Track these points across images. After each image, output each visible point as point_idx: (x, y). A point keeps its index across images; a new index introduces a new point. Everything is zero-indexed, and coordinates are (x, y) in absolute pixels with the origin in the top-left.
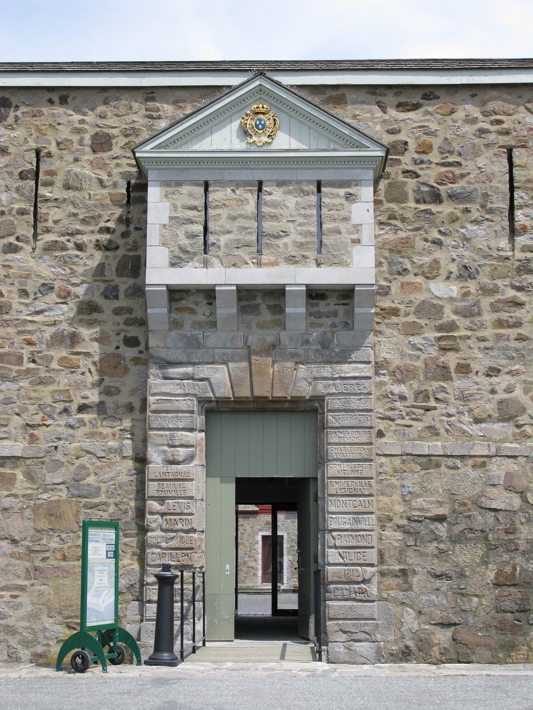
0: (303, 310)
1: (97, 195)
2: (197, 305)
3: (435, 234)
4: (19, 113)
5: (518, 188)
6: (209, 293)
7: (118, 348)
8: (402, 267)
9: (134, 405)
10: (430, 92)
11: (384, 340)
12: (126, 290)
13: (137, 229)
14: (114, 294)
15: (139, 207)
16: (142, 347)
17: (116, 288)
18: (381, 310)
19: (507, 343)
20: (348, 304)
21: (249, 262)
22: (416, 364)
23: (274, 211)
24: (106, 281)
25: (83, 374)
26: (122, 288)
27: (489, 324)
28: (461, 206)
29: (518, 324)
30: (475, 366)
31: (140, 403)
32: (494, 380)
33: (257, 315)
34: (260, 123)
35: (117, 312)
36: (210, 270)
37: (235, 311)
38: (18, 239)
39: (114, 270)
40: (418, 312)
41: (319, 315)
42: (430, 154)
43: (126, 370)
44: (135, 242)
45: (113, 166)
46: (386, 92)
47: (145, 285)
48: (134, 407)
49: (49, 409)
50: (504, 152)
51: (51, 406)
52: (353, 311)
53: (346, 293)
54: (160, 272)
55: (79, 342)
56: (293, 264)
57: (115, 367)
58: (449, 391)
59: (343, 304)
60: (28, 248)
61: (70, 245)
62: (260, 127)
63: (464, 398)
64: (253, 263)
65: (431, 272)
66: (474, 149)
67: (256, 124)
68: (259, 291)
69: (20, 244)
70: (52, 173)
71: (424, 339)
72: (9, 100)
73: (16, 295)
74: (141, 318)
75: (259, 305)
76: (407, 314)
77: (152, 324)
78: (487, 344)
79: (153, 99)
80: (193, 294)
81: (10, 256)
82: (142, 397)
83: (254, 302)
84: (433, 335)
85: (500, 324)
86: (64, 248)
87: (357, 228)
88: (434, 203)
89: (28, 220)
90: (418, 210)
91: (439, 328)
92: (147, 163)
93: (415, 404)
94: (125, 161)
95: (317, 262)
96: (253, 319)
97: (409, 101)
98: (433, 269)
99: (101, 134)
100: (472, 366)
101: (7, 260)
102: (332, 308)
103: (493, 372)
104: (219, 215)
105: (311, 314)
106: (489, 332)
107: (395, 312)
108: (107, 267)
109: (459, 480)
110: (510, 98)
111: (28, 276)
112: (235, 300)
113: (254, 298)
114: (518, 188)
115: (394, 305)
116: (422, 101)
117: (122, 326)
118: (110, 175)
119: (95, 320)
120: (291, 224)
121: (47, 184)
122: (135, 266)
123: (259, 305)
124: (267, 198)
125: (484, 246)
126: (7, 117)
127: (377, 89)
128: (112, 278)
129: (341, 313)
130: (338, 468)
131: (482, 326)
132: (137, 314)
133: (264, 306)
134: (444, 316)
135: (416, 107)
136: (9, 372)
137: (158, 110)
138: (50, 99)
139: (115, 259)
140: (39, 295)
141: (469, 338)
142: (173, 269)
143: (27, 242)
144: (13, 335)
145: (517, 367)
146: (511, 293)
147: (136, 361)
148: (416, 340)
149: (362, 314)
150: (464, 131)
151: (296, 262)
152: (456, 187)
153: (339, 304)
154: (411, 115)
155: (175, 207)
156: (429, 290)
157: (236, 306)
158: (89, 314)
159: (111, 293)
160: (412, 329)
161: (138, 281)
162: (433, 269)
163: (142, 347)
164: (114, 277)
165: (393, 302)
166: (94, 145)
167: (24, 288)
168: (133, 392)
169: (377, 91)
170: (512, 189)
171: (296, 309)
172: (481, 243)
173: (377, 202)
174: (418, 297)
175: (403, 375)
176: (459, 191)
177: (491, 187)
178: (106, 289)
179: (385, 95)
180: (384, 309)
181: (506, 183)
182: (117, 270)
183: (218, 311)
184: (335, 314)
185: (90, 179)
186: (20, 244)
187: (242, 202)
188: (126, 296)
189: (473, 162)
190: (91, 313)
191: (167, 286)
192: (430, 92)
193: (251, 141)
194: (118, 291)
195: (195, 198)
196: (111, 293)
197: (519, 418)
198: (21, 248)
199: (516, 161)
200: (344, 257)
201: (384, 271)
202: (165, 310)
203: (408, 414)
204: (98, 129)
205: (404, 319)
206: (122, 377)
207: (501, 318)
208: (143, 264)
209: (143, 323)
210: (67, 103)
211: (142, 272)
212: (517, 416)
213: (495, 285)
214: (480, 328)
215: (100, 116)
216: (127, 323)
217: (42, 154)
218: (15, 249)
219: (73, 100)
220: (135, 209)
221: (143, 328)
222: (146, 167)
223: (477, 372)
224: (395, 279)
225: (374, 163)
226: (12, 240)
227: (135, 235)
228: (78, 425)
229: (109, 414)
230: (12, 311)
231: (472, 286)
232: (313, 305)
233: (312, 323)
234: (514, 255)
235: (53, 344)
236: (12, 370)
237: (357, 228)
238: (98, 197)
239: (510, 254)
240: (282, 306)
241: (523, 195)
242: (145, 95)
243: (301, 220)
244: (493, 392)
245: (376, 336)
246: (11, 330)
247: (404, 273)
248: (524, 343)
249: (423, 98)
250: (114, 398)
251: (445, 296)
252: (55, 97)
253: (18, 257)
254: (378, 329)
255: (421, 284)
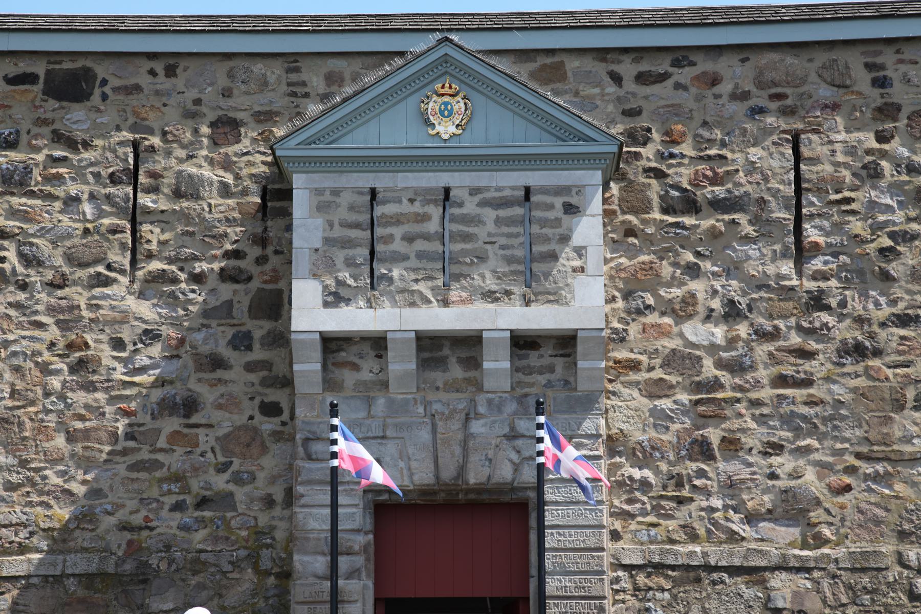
0: (507, 365)
1: (220, 205)
2: (361, 358)
3: (690, 257)
4: (107, 89)
5: (808, 190)
6: (378, 343)
7: (251, 418)
8: (643, 302)
9: (274, 497)
10: (683, 57)
11: (620, 404)
12: (263, 337)
13: (277, 252)
14: (246, 343)
15: (281, 222)
16: (285, 416)
17: (248, 336)
18: (615, 362)
19: (792, 407)
20: (569, 356)
21: (433, 299)
22: (664, 437)
23: (466, 229)
24: (234, 325)
25: (202, 455)
26: (257, 334)
27: (765, 381)
28: (726, 217)
29: (807, 383)
30: (747, 441)
31: (283, 495)
32: (776, 460)
33: (444, 372)
34: (446, 109)
35: (250, 367)
36: (379, 311)
37: (414, 367)
38: (109, 267)
39: (246, 309)
40: (665, 365)
41: (529, 371)
42: (684, 145)
43: (264, 450)
44: (274, 270)
45: (242, 165)
46: (622, 57)
47: (290, 332)
48: (274, 501)
49: (154, 505)
50: (787, 140)
51: (158, 501)
52: (575, 364)
53: (566, 342)
54: (311, 312)
55: (197, 411)
56: (492, 302)
57: (248, 445)
58: (711, 475)
59: (562, 355)
60: (124, 280)
61: (183, 276)
62: (446, 113)
63: (731, 486)
64: (438, 301)
65: (684, 310)
66: (745, 136)
67: (440, 109)
68: (445, 338)
69: (113, 275)
70: (154, 175)
71: (675, 402)
72: (93, 71)
73: (106, 347)
74: (284, 376)
75: (447, 357)
76: (651, 369)
77: (300, 386)
78: (766, 411)
79: (297, 70)
80: (356, 343)
81: (97, 291)
82: (285, 486)
83: (440, 353)
84: (684, 397)
85: (781, 381)
86: (175, 281)
87: (580, 251)
88: (688, 212)
89: (124, 241)
90: (665, 223)
91: (698, 387)
92: (291, 165)
93: (663, 493)
94: (259, 158)
95: (525, 299)
96: (438, 377)
97: (653, 69)
98: (688, 304)
99: (224, 119)
100: (743, 440)
101: (94, 297)
102: (546, 361)
103: (775, 448)
104: (392, 235)
105: (518, 370)
106: (766, 393)
107: (634, 366)
108: (236, 306)
109: (727, 602)
110: (796, 62)
111: (124, 322)
112: (414, 352)
113: (440, 348)
114: (808, 190)
115: (633, 356)
116: (671, 70)
117: (259, 388)
118: (237, 177)
119: (219, 380)
120: (488, 247)
121: (148, 191)
122: (275, 305)
123: (447, 357)
124: (456, 211)
125: (758, 272)
126: (91, 94)
127: (608, 53)
128: (243, 321)
129: (559, 369)
130: (557, 584)
131: (757, 384)
132: (280, 369)
133: (453, 360)
134: (704, 370)
135: (663, 78)
136: (97, 455)
137: (304, 84)
138: (152, 69)
139: (246, 294)
140: (140, 345)
141: (738, 401)
142: (329, 310)
143: (122, 272)
144: (103, 402)
145: (808, 441)
146: (795, 339)
147: (277, 436)
148: (665, 404)
149: (588, 369)
150: (731, 111)
151: (497, 300)
152: (719, 191)
153: (556, 356)
154: (656, 89)
155: (331, 225)
156: (681, 335)
157: (415, 360)
158: (210, 372)
159: (242, 341)
160: (656, 390)
161: (279, 325)
162: (688, 304)
163: (285, 416)
164: (246, 319)
165: (632, 351)
166: (215, 136)
167: (119, 335)
168: (273, 480)
169: (609, 56)
170: (799, 191)
171: (497, 364)
172: (753, 269)
173: (608, 214)
174: (666, 344)
175: (644, 456)
176: (723, 196)
177: (769, 189)
178: (234, 336)
179: (619, 62)
180: (620, 362)
181: (790, 184)
182: (250, 311)
183: (391, 367)
184: (551, 369)
185: (211, 183)
186: (113, 275)
187: (425, 218)
188: (262, 345)
189: (743, 155)
190: (214, 370)
191: (320, 332)
192: (683, 57)
193: (434, 132)
194: (251, 338)
195: (358, 212)
196: (242, 341)
197: (812, 514)
198: (115, 281)
199: (805, 152)
200: (563, 293)
201: (618, 309)
202: (318, 366)
203: (653, 508)
204: (221, 113)
205: (647, 376)
206: (258, 458)
207: (784, 372)
208: (286, 301)
209: (287, 382)
210: (175, 75)
211: (284, 313)
212: (809, 511)
213: (776, 328)
214: (754, 387)
215: (223, 95)
216: (264, 383)
217: (142, 148)
218: (107, 282)
219: (185, 70)
220: (274, 226)
221: (287, 391)
222: (290, 169)
223: (751, 449)
224: (633, 320)
225: (603, 161)
226: (101, 269)
227: (274, 261)
228: (196, 527)
229: (240, 511)
230: (101, 368)
231: (743, 330)
232: (520, 358)
233: (519, 382)
234: (801, 284)
235: (161, 415)
236: (101, 451)
237: (580, 251)
238: (222, 208)
239: (795, 282)
240: (479, 358)
241: (814, 200)
242: (286, 65)
243: (503, 241)
244: (773, 476)
245: (609, 398)
246: (100, 396)
247: (647, 312)
248: (818, 409)
249: (673, 65)
250: (247, 489)
251: (705, 343)
252: (159, 67)
253: (110, 292)
254: (611, 389)
255: (670, 326)
